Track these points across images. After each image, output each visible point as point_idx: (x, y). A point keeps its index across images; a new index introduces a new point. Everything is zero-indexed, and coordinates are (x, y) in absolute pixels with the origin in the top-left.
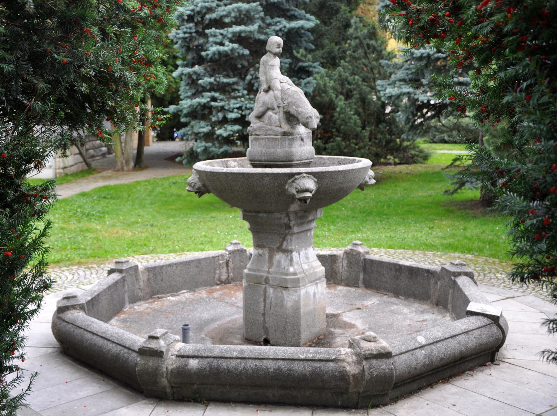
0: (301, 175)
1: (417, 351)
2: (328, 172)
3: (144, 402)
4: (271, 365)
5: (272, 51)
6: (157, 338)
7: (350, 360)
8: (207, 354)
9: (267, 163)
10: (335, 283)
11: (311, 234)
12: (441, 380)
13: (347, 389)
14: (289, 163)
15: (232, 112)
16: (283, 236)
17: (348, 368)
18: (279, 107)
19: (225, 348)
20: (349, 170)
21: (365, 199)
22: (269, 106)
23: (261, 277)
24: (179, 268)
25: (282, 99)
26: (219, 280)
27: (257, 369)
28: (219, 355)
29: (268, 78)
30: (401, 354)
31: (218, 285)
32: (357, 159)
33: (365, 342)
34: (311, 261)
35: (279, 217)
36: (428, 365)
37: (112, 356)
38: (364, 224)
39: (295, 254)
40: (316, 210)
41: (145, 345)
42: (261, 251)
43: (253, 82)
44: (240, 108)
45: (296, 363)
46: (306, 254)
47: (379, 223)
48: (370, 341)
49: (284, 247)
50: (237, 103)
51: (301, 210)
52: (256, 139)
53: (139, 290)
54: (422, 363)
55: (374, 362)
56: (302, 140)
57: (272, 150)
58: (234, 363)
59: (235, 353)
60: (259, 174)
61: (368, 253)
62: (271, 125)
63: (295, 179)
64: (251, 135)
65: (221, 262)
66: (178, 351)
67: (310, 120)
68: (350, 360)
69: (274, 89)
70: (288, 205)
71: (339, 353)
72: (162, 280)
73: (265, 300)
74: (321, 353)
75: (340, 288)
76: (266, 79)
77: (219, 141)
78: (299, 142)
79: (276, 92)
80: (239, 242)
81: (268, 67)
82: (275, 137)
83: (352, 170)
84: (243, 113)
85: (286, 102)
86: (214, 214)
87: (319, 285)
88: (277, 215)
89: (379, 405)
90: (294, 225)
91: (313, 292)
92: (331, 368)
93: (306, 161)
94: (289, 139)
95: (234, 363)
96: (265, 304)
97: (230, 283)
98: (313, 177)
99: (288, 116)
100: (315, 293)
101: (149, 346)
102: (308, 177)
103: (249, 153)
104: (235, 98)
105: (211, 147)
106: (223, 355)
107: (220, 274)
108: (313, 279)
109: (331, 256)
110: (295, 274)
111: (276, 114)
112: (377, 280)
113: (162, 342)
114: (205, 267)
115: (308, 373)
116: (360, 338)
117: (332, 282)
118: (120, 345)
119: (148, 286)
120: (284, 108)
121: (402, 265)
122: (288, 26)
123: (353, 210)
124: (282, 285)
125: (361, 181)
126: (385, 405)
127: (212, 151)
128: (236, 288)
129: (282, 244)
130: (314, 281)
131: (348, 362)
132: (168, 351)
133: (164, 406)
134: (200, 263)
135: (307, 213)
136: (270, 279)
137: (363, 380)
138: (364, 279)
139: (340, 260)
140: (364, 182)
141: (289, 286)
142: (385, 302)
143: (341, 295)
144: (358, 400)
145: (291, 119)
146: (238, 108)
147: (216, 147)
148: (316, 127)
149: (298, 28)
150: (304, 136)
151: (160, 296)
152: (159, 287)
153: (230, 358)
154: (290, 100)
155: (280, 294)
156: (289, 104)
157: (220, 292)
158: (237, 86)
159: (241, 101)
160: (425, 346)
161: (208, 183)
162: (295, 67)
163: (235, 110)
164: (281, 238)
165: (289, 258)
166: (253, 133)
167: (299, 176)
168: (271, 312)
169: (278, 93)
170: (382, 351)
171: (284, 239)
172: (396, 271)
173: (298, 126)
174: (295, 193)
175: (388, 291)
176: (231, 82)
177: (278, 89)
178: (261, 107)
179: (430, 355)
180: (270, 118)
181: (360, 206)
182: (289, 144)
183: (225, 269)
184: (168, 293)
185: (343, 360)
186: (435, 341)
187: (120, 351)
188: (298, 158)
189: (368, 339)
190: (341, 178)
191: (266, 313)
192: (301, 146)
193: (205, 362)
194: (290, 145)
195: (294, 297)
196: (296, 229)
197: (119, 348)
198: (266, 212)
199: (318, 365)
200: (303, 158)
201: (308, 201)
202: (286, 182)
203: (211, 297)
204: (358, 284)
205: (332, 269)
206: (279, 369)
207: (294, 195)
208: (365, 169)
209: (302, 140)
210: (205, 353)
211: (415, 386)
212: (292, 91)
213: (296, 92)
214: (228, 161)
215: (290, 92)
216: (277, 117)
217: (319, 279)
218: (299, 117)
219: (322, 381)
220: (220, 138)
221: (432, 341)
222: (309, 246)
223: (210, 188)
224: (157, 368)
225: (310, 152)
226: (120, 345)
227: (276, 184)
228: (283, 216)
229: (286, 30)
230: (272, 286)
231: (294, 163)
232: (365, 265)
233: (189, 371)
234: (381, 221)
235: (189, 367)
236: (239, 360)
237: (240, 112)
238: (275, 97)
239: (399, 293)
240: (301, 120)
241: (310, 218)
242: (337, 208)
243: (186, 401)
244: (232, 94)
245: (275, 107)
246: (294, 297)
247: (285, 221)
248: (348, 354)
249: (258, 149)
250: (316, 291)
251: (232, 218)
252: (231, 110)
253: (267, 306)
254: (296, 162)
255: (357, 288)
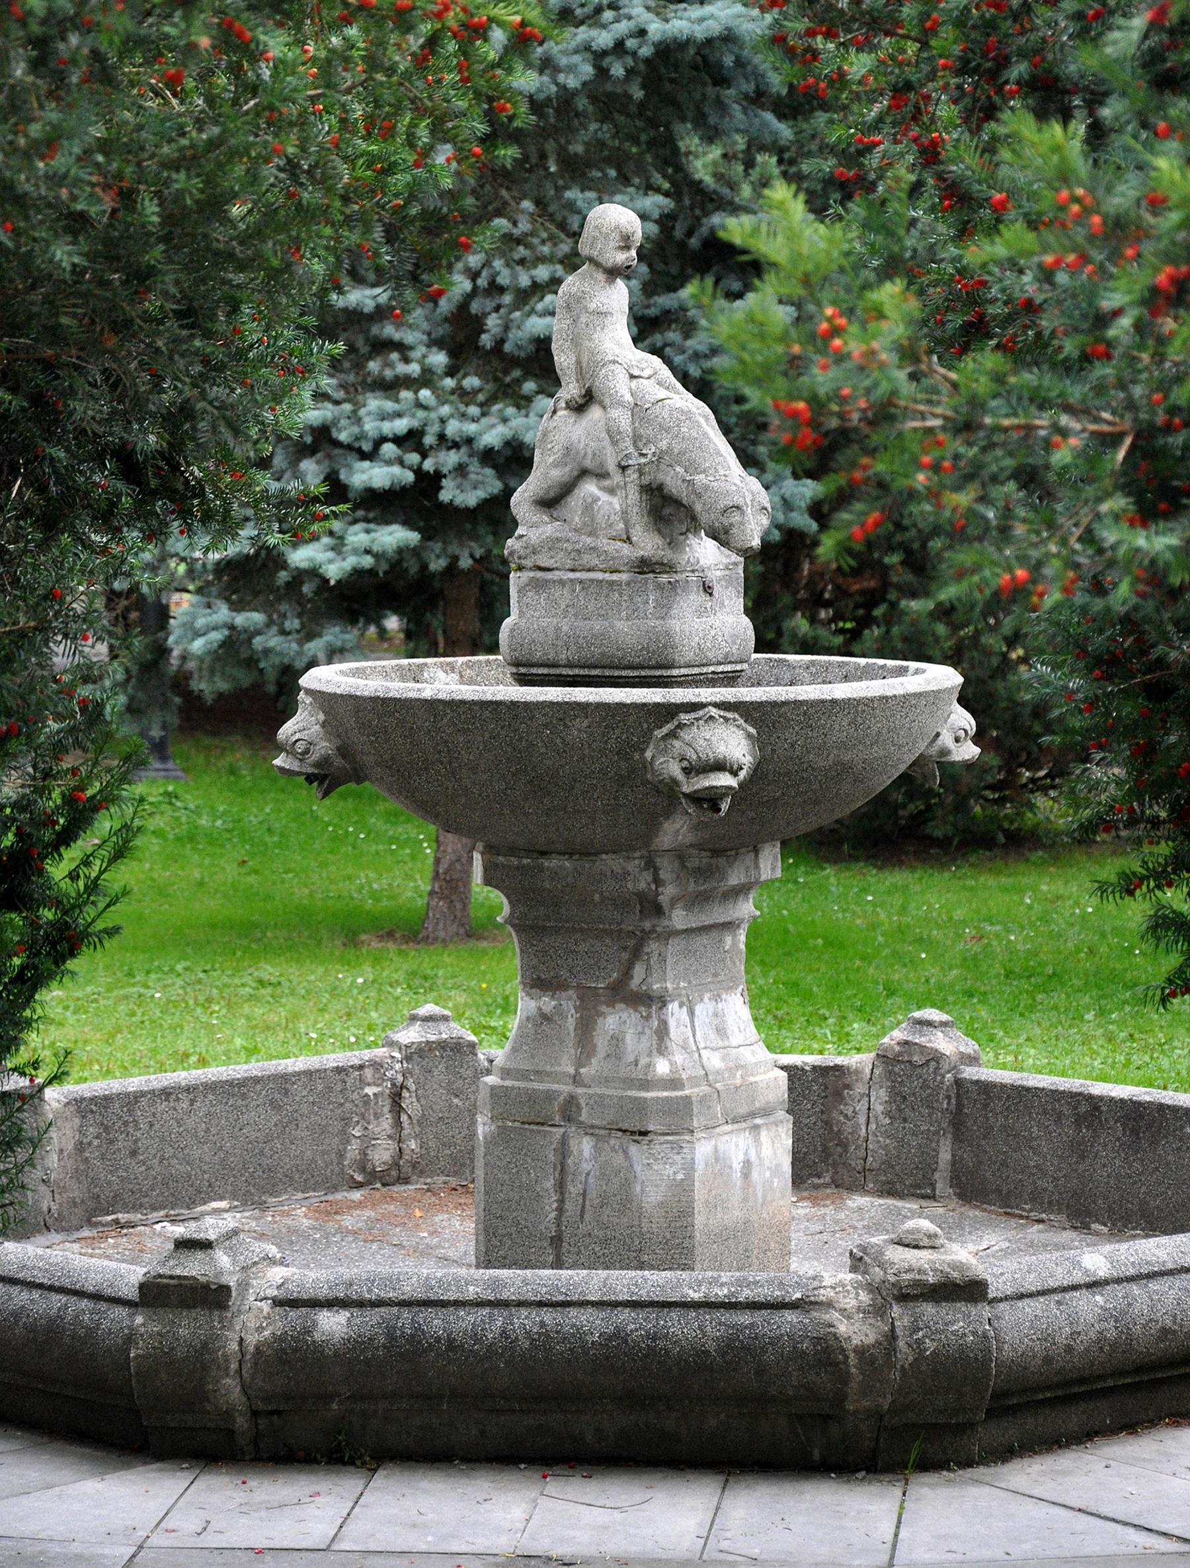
0: (701, 713)
1: (1076, 1294)
2: (797, 704)
3: (154, 1466)
4: (593, 1323)
5: (600, 259)
6: (205, 1245)
7: (850, 1303)
8: (376, 1293)
9: (577, 671)
10: (837, 1184)
11: (735, 944)
12: (1169, 1415)
13: (841, 1398)
14: (658, 673)
15: (370, 456)
16: (631, 943)
17: (843, 1328)
18: (624, 468)
19: (439, 1275)
20: (872, 700)
21: (1045, 919)
22: (588, 463)
23: (550, 1096)
24: (201, 1107)
25: (636, 439)
26: (363, 1164)
27: (547, 1335)
28: (420, 1295)
29: (585, 360)
30: (1021, 1296)
31: (359, 1186)
32: (913, 665)
33: (901, 1248)
34: (734, 1043)
35: (618, 869)
36: (1114, 1345)
37: (31, 1329)
38: (1017, 1022)
39: (676, 1014)
40: (756, 851)
41: (164, 1271)
42: (547, 1003)
43: (475, 307)
44: (411, 440)
45: (675, 1314)
46: (716, 1015)
47: (1089, 1016)
48: (916, 1247)
49: (635, 983)
50: (399, 415)
51: (700, 847)
52: (537, 585)
53: (42, 1188)
54: (1093, 1335)
55: (928, 1310)
56: (708, 590)
57: (597, 625)
58: (471, 1318)
59: (471, 1288)
60: (552, 704)
61: (973, 1060)
62: (592, 534)
63: (680, 726)
64: (520, 568)
65: (370, 1091)
66: (279, 1287)
67: (736, 518)
68: (850, 1303)
69: (607, 401)
70: (653, 825)
71: (816, 1284)
72: (134, 1153)
73: (561, 1186)
74: (756, 1283)
75: (858, 1201)
76: (579, 362)
77: (301, 600)
78: (696, 598)
79: (615, 413)
80: (446, 1012)
81: (583, 319)
82: (607, 576)
83: (884, 699)
84: (428, 465)
85: (650, 450)
86: (268, 971)
87: (764, 1134)
88: (611, 863)
89: (948, 1462)
90: (673, 902)
91: (741, 1157)
92: (786, 1328)
93: (720, 669)
94: (660, 587)
95: (471, 1318)
96: (561, 1201)
97: (406, 1181)
98: (741, 721)
99: (657, 501)
100: (747, 1164)
101: (178, 1272)
102: (726, 720)
103: (511, 636)
104: (389, 387)
105: (259, 632)
106: (433, 1297)
107: (368, 1141)
108: (743, 1110)
109: (822, 1071)
110: (674, 1083)
111: (611, 491)
112: (1004, 1164)
113: (223, 1259)
114: (305, 1109)
115: (711, 1346)
116: (885, 1241)
117: (827, 1179)
118: (61, 1290)
119: (77, 1174)
120: (641, 474)
121: (1101, 1098)
122: (656, 28)
123: (971, 962)
124: (625, 1126)
125: (921, 747)
126: (968, 1463)
127: (267, 652)
128: (429, 1199)
129: (627, 974)
130: (744, 1118)
131: (843, 1311)
132: (244, 1286)
133: (227, 1473)
134: (286, 1092)
135: (722, 861)
136: (583, 1102)
137: (890, 1365)
138: (954, 1163)
139: (860, 1088)
140: (933, 751)
141: (651, 1128)
142: (1031, 1245)
143: (859, 1225)
144: (877, 1439)
145: (667, 511)
146: (398, 440)
147: (284, 632)
148: (756, 542)
149: (709, 41)
150: (714, 575)
151: (123, 1217)
152: (122, 1179)
153: (457, 1304)
154: (663, 445)
155: (619, 1159)
156: (660, 457)
157: (369, 1213)
158: (398, 326)
159: (419, 405)
160: (1105, 1282)
161: (360, 741)
162: (690, 233)
163: (389, 449)
164: (625, 949)
165: (655, 1023)
166: (528, 563)
167: (693, 715)
168: (583, 1228)
169: (622, 419)
170: (955, 1274)
171: (636, 953)
172: (1079, 1120)
173: (692, 540)
174: (680, 776)
175: (1050, 1206)
176: (369, 306)
177: (620, 404)
178: (556, 465)
179: (1124, 1313)
180: (589, 507)
181: (1010, 948)
182: (658, 605)
183: (386, 1123)
184: (154, 1209)
185: (829, 1305)
186: (1144, 1271)
187: (66, 1307)
188: (690, 656)
189: (909, 1239)
190: (841, 727)
191: (566, 1237)
192: (701, 612)
193: (373, 1317)
194: (664, 610)
195: (669, 1171)
196: (679, 918)
197: (58, 1300)
198: (570, 854)
199: (745, 1318)
200: (710, 655)
201: (725, 806)
202: (647, 736)
203: (331, 1226)
204: (933, 1186)
205: (828, 1124)
206: (619, 1335)
207: (675, 782)
208: (931, 699)
209: (708, 590)
210: (370, 1291)
211: (1074, 1418)
212: (672, 410)
213: (687, 414)
214: (421, 667)
215: (665, 415)
216: (616, 502)
217: (766, 1112)
218: (698, 507)
219: (760, 1372)
220: (307, 589)
221: (1131, 1272)
222: (730, 989)
223: (369, 760)
224: (205, 1345)
225: (735, 636)
226: (61, 1290)
227: (612, 744)
228: (633, 866)
229: (646, 51)
230: (589, 1130)
231: (675, 672)
232: (959, 1106)
233: (318, 1347)
234: (1102, 1013)
235: (317, 1336)
236: (486, 1311)
237: (413, 458)
238: (608, 431)
239: (1088, 1214)
240: (704, 518)
241: (735, 878)
242: (895, 953)
243: (299, 1461)
244: (373, 366)
245: (611, 466)
246: (669, 1171)
247: (642, 885)
248: (844, 1286)
249: (544, 622)
250: (753, 1156)
251: (362, 989)
252: (366, 447)
253: (568, 1205)
254: (683, 671)
255: (924, 1203)
